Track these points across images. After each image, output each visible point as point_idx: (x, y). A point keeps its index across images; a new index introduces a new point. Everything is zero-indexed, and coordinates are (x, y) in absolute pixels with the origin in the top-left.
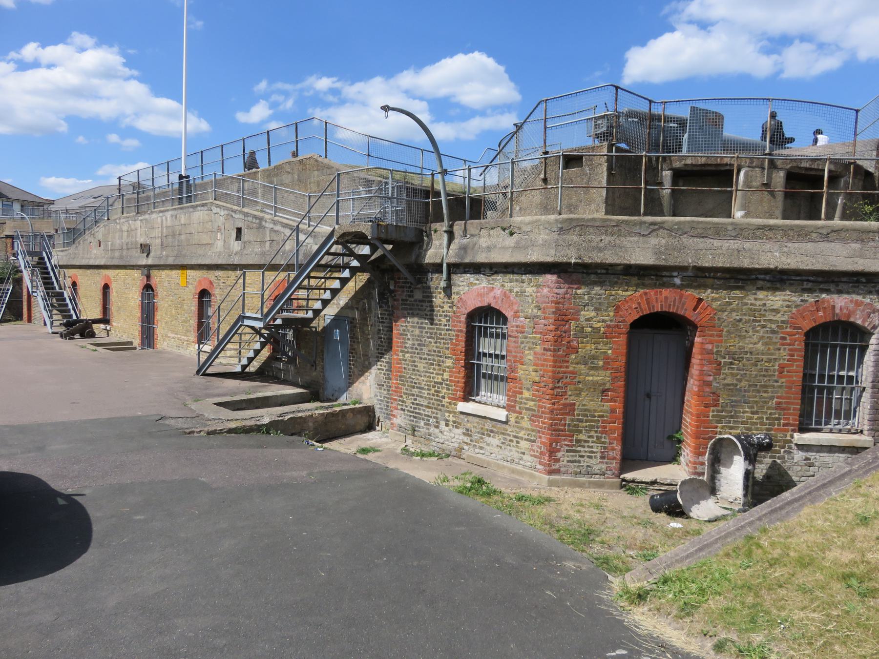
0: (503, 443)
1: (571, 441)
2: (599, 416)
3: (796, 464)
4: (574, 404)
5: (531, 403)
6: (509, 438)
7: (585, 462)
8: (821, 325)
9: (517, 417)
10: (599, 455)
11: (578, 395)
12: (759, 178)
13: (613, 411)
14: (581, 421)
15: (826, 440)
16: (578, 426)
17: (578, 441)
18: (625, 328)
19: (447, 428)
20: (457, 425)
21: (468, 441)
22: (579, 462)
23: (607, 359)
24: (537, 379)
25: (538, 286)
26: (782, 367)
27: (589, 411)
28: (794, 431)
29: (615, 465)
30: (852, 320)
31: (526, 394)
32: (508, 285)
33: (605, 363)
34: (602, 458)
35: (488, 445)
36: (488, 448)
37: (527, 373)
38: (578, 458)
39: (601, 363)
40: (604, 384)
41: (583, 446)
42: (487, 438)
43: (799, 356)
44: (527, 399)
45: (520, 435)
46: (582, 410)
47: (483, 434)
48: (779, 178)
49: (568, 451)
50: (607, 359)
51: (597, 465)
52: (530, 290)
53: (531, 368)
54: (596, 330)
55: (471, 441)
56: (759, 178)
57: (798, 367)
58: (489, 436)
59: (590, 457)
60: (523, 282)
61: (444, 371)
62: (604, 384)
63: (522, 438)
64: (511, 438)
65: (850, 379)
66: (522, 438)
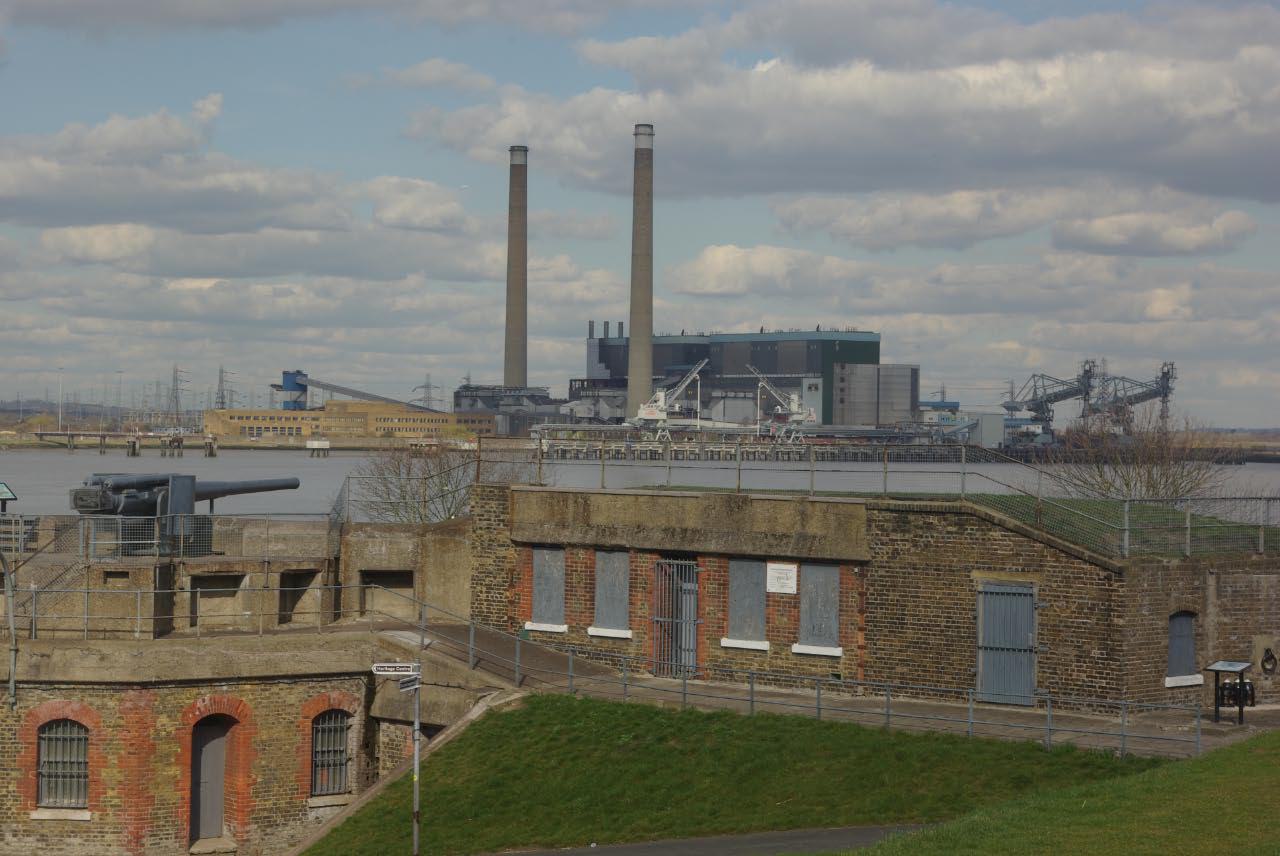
0: (86, 841)
1: (152, 827)
2: (174, 804)
3: (311, 822)
4: (154, 797)
5: (117, 800)
6: (92, 835)
7: (164, 843)
8: (320, 714)
9: (101, 815)
10: (173, 836)
11: (158, 788)
12: (261, 580)
13: (183, 798)
14: (160, 809)
15: (405, 643)
16: (156, 814)
17: (158, 826)
18: (189, 729)
19: (15, 839)
20: (27, 833)
21: (44, 847)
22: (159, 843)
23: (178, 756)
24: (122, 779)
25: (121, 700)
26: (298, 748)
27: (165, 800)
28: (307, 797)
29: (185, 842)
30: (341, 707)
31: (110, 793)
32: (88, 699)
33: (176, 760)
34: (176, 838)
35: (68, 845)
36: (68, 848)
37: (110, 775)
38: (158, 841)
39: (173, 760)
40: (176, 777)
41: (162, 830)
42: (68, 840)
43: (308, 739)
44: (111, 797)
45: (106, 830)
46: (161, 801)
47: (63, 836)
48: (275, 579)
49: (151, 836)
50: (178, 756)
51: (171, 843)
52: (111, 704)
53: (115, 771)
54: (169, 733)
55: (47, 845)
56: (261, 580)
57: (307, 747)
58: (70, 837)
59: (167, 839)
60: (104, 696)
61: (9, 783)
62: (176, 777)
63: (107, 833)
64: (96, 834)
65: (341, 752)
66: (107, 833)
